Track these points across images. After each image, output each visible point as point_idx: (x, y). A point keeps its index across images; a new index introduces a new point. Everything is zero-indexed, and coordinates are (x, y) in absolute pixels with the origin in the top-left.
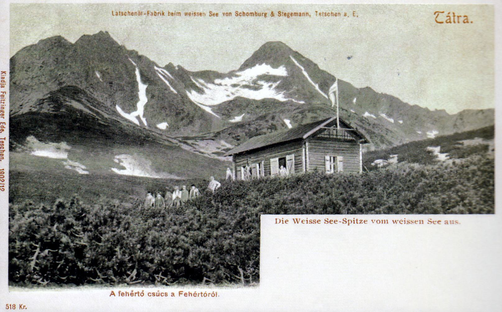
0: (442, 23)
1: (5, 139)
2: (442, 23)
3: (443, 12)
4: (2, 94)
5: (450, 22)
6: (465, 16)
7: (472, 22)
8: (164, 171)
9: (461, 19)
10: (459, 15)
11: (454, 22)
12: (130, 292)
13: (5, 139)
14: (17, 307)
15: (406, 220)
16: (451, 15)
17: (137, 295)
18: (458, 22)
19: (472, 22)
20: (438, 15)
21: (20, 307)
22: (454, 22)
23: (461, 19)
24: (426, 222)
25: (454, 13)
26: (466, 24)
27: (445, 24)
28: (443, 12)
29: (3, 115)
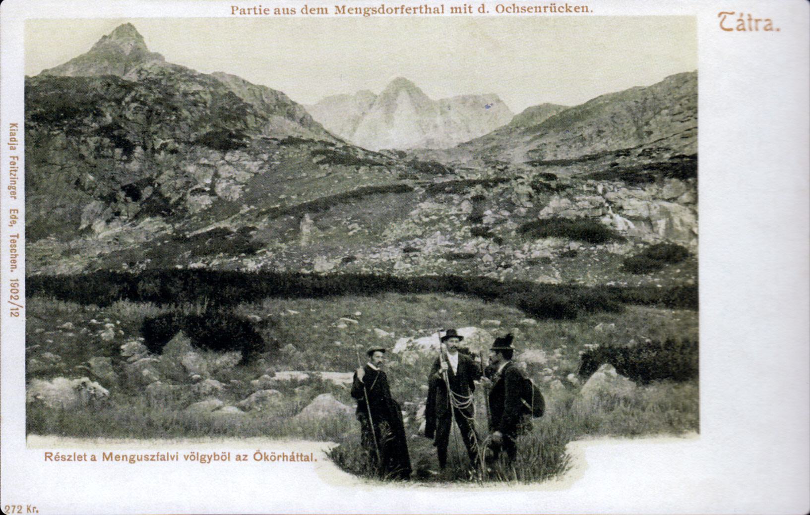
0: (731, 30)
1: (18, 236)
2: (731, 30)
3: (732, 13)
4: (12, 160)
5: (744, 29)
6: (767, 20)
7: (778, 30)
8: (326, 277)
9: (761, 25)
10: (757, 18)
11: (751, 29)
12: (289, 454)
13: (18, 236)
14: (24, 509)
15: (77, 455)
16: (745, 18)
17: (281, 459)
18: (757, 29)
19: (778, 30)
20: (725, 17)
21: (28, 509)
22: (751, 29)
23: (761, 25)
24: (99, 457)
25: (749, 15)
26: (769, 33)
27: (735, 31)
28: (732, 13)
29: (15, 193)
